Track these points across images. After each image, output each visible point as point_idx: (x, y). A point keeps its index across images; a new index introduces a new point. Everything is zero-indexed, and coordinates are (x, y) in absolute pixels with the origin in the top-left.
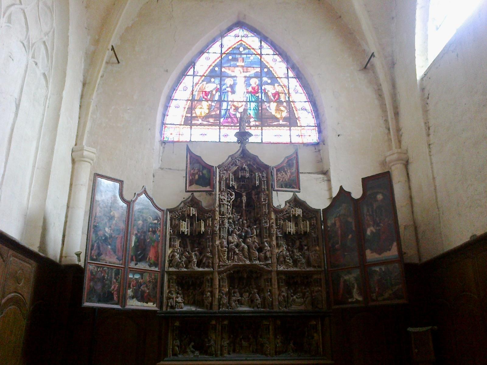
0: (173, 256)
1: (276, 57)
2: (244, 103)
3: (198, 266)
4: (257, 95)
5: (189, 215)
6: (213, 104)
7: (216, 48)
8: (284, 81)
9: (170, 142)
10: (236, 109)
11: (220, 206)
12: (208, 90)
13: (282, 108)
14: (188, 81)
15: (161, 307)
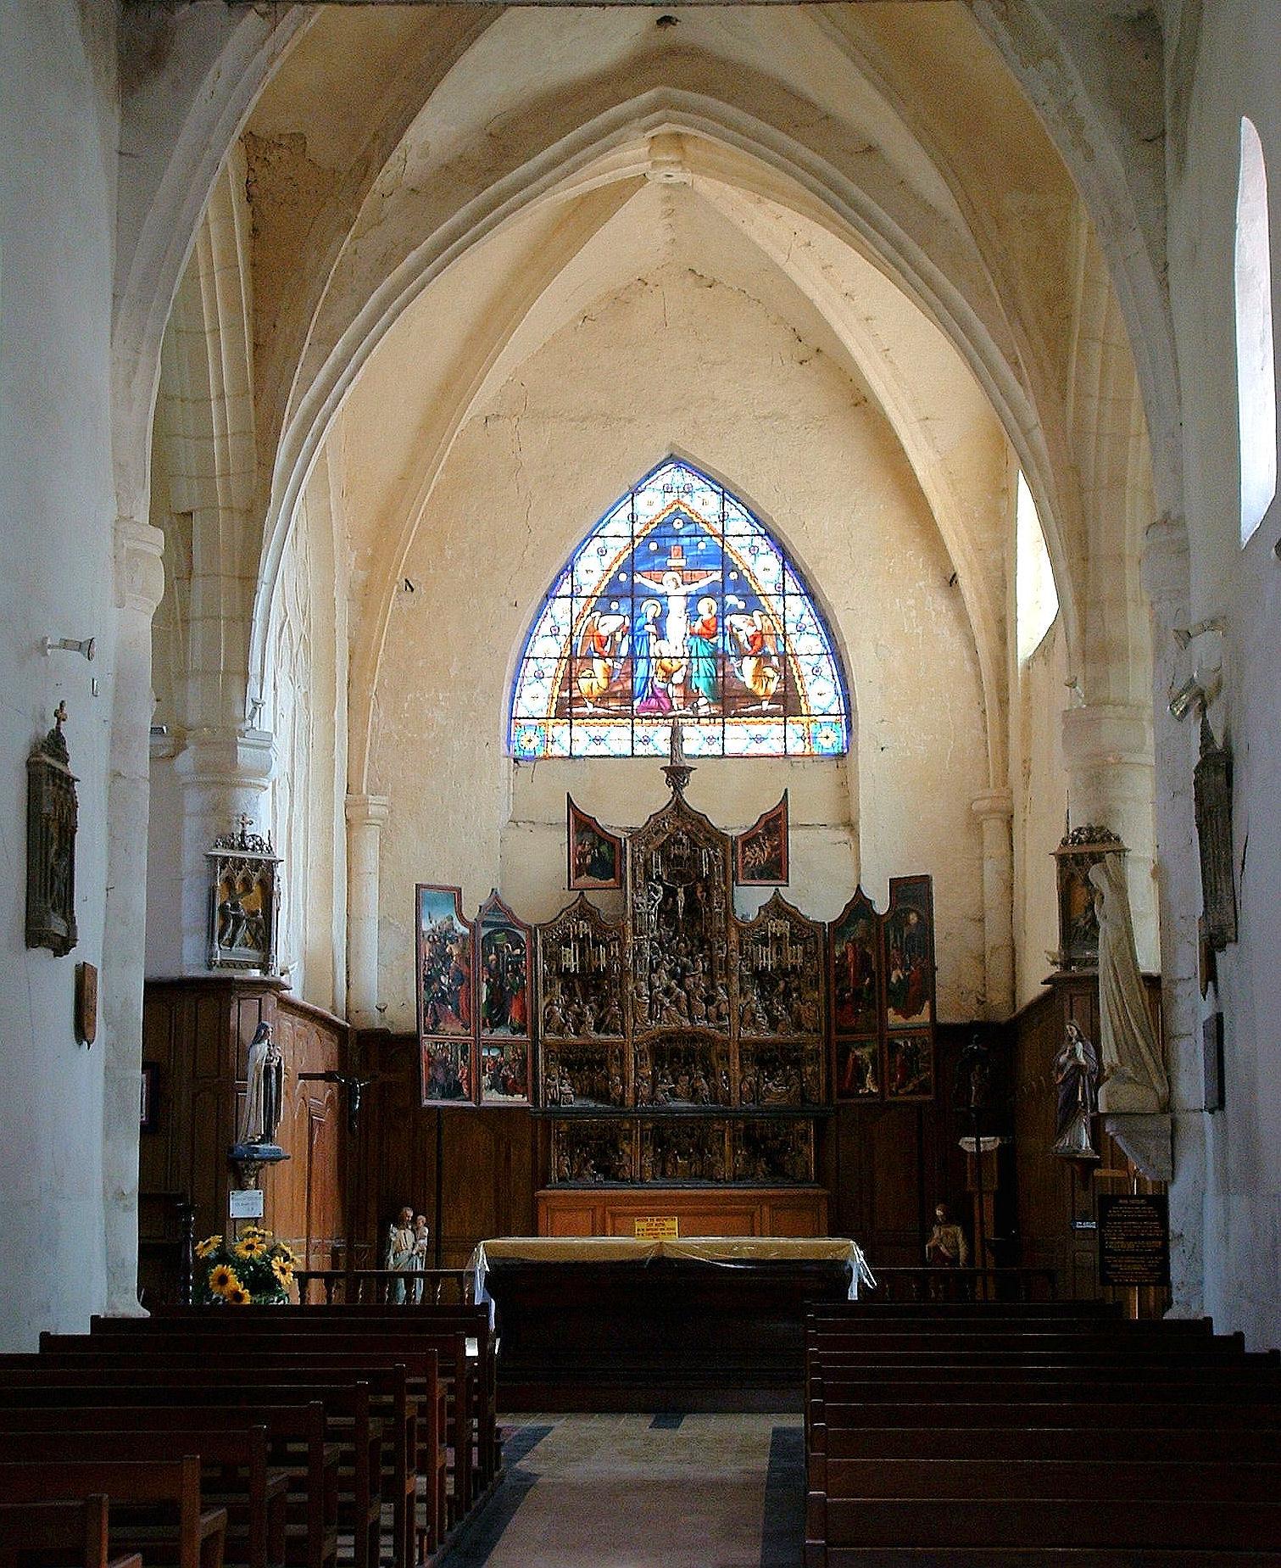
0: (552, 1013)
1: (758, 541)
2: (685, 662)
3: (597, 1029)
4: (713, 640)
5: (576, 937)
6: (617, 666)
7: (619, 524)
8: (775, 604)
9: (527, 759)
10: (669, 675)
11: (634, 916)
12: (604, 632)
13: (770, 672)
14: (560, 608)
15: (535, 1101)
